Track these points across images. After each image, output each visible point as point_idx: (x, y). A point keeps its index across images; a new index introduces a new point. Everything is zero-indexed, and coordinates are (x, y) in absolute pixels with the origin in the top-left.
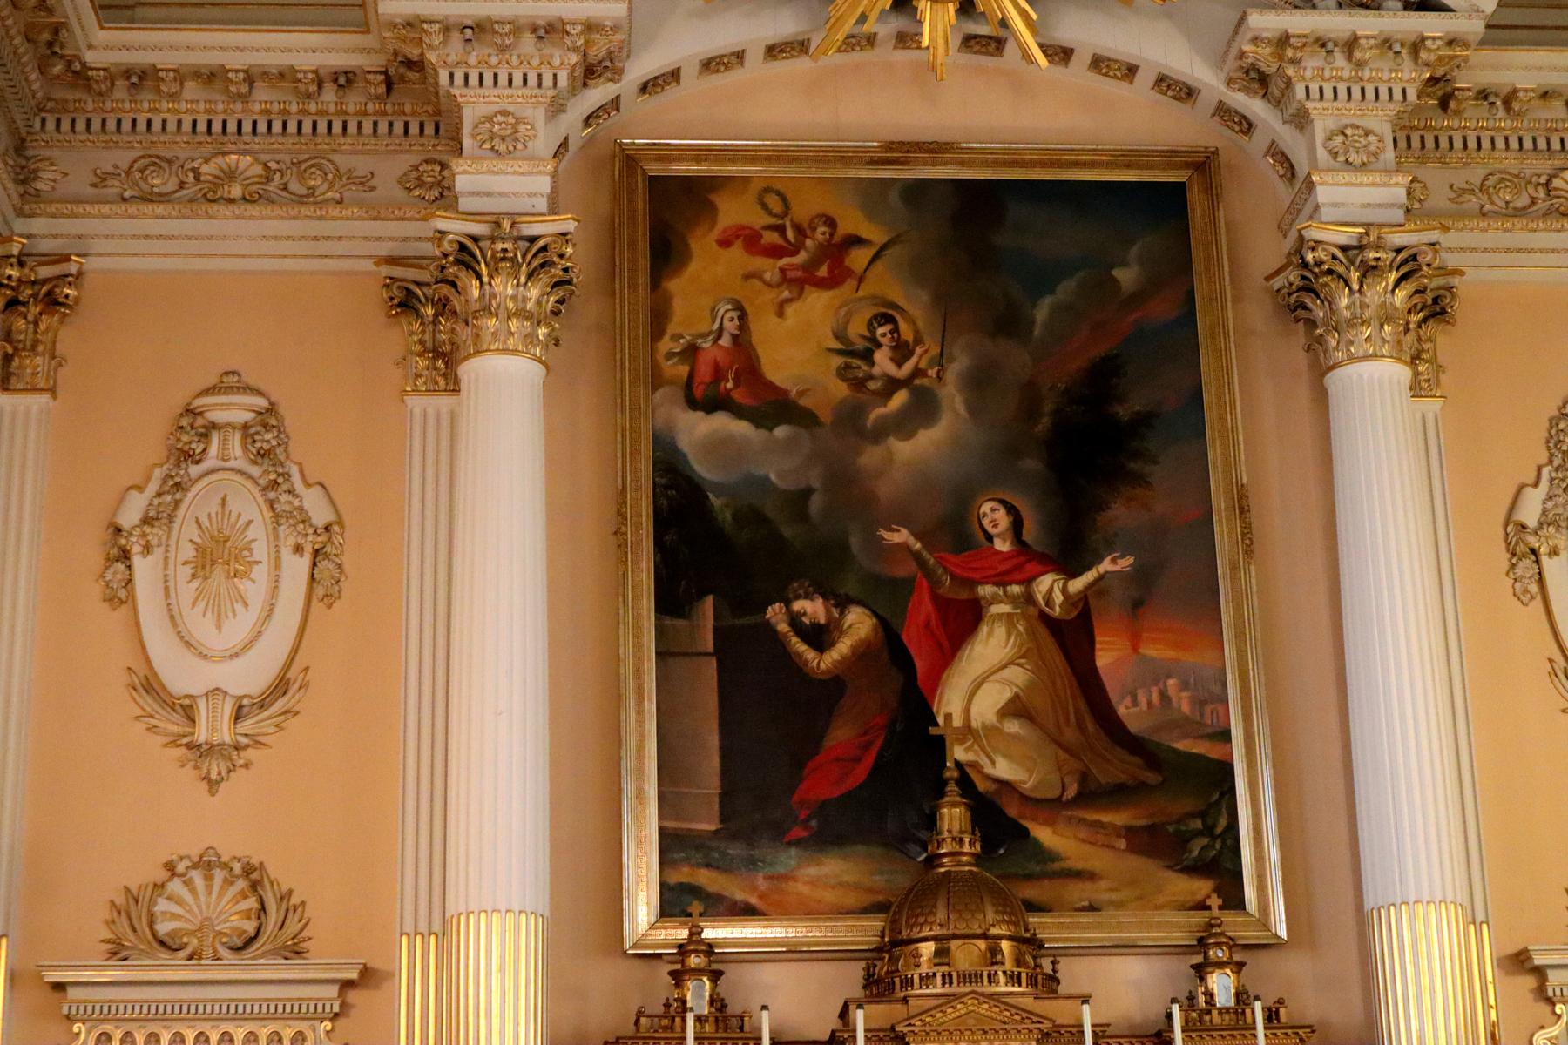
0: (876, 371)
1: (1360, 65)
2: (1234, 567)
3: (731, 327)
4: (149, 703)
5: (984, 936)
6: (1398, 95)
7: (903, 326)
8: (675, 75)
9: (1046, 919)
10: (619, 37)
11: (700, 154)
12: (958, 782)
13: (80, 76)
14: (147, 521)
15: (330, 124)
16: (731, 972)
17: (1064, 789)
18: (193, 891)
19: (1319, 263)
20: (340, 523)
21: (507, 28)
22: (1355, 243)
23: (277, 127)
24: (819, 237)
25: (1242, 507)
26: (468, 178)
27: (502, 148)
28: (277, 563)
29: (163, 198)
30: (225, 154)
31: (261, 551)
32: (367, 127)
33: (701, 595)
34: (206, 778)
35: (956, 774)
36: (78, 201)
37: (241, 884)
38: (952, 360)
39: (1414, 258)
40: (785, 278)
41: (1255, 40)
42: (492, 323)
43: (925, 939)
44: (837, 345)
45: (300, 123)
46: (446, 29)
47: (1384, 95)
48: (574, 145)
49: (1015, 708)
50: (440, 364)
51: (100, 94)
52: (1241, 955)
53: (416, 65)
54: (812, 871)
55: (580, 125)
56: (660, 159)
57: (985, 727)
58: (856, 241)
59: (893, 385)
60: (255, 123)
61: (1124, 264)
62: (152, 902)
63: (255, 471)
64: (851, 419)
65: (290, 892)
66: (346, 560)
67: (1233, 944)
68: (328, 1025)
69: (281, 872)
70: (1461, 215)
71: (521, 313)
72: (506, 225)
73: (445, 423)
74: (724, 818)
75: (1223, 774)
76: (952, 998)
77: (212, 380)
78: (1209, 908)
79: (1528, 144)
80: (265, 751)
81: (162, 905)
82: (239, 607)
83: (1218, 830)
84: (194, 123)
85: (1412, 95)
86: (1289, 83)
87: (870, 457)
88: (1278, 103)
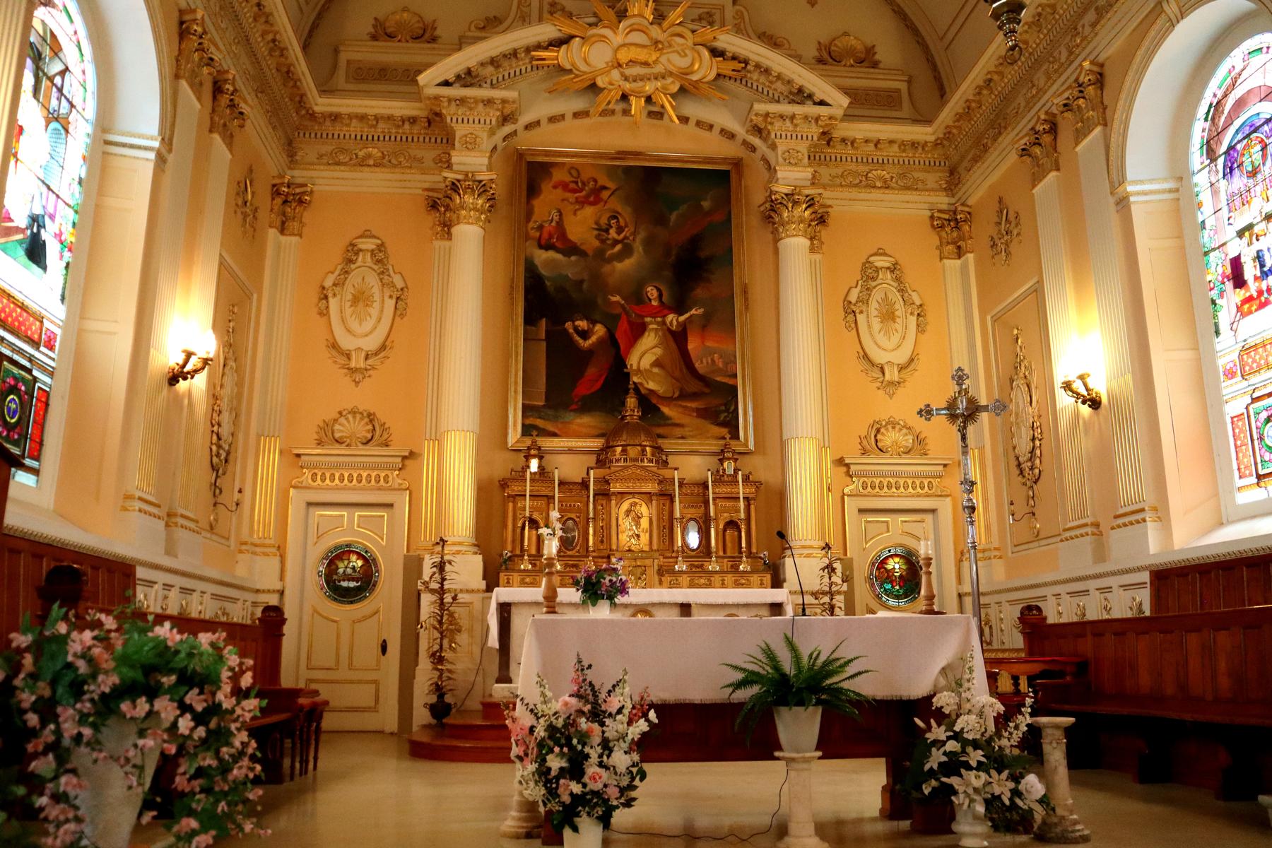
0: (610, 237)
1: (796, 125)
2: (741, 313)
3: (556, 218)
4: (334, 352)
5: (640, 445)
6: (810, 138)
7: (621, 220)
8: (538, 123)
9: (666, 441)
10: (515, 106)
11: (547, 153)
12: (634, 389)
13: (312, 116)
14: (335, 285)
15: (407, 138)
16: (547, 457)
17: (674, 393)
18: (349, 422)
19: (776, 200)
20: (407, 288)
21: (472, 100)
22: (790, 192)
23: (387, 138)
24: (591, 186)
25: (745, 292)
26: (457, 158)
27: (470, 146)
28: (383, 302)
29: (344, 164)
30: (367, 148)
31: (377, 297)
32: (421, 139)
33: (541, 318)
34: (354, 381)
35: (633, 386)
36: (312, 164)
37: (366, 420)
38: (639, 233)
39: (813, 199)
40: (577, 201)
41: (756, 115)
42: (464, 212)
43: (618, 446)
44: (596, 227)
45: (396, 137)
46: (450, 100)
47: (805, 138)
48: (499, 148)
49: (657, 363)
50: (446, 229)
51: (320, 123)
52: (737, 456)
53: (438, 115)
54: (578, 421)
55: (501, 140)
56: (532, 155)
57: (645, 370)
58: (604, 188)
59: (616, 242)
60: (379, 137)
61: (705, 200)
62: (333, 425)
63: (376, 267)
64: (600, 255)
65: (384, 423)
66: (408, 301)
67: (734, 452)
68: (397, 472)
70: (835, 186)
71: (475, 209)
72: (470, 175)
73: (447, 250)
74: (547, 398)
75: (734, 389)
76: (626, 468)
77: (360, 234)
78: (725, 439)
79: (860, 160)
80: (376, 371)
81: (337, 427)
82: (368, 318)
83: (731, 410)
84: (356, 136)
85: (815, 138)
86: (769, 133)
87: (606, 269)
88: (765, 140)
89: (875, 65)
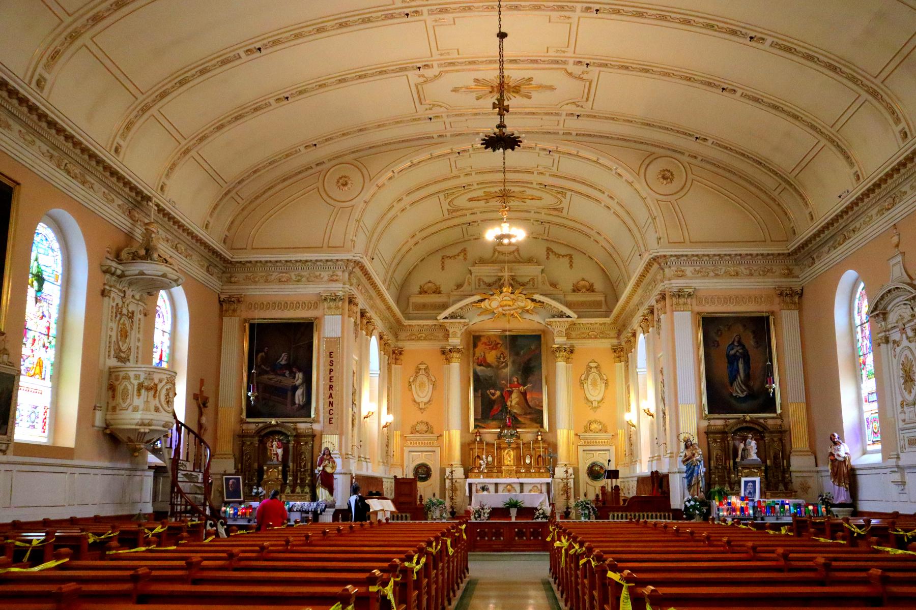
58: (498, 344)
59: (503, 362)
69: (430, 423)
89: (593, 291)
